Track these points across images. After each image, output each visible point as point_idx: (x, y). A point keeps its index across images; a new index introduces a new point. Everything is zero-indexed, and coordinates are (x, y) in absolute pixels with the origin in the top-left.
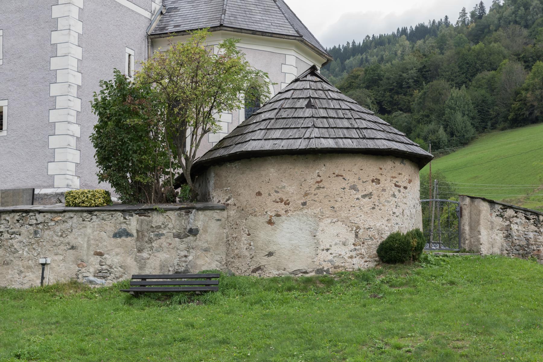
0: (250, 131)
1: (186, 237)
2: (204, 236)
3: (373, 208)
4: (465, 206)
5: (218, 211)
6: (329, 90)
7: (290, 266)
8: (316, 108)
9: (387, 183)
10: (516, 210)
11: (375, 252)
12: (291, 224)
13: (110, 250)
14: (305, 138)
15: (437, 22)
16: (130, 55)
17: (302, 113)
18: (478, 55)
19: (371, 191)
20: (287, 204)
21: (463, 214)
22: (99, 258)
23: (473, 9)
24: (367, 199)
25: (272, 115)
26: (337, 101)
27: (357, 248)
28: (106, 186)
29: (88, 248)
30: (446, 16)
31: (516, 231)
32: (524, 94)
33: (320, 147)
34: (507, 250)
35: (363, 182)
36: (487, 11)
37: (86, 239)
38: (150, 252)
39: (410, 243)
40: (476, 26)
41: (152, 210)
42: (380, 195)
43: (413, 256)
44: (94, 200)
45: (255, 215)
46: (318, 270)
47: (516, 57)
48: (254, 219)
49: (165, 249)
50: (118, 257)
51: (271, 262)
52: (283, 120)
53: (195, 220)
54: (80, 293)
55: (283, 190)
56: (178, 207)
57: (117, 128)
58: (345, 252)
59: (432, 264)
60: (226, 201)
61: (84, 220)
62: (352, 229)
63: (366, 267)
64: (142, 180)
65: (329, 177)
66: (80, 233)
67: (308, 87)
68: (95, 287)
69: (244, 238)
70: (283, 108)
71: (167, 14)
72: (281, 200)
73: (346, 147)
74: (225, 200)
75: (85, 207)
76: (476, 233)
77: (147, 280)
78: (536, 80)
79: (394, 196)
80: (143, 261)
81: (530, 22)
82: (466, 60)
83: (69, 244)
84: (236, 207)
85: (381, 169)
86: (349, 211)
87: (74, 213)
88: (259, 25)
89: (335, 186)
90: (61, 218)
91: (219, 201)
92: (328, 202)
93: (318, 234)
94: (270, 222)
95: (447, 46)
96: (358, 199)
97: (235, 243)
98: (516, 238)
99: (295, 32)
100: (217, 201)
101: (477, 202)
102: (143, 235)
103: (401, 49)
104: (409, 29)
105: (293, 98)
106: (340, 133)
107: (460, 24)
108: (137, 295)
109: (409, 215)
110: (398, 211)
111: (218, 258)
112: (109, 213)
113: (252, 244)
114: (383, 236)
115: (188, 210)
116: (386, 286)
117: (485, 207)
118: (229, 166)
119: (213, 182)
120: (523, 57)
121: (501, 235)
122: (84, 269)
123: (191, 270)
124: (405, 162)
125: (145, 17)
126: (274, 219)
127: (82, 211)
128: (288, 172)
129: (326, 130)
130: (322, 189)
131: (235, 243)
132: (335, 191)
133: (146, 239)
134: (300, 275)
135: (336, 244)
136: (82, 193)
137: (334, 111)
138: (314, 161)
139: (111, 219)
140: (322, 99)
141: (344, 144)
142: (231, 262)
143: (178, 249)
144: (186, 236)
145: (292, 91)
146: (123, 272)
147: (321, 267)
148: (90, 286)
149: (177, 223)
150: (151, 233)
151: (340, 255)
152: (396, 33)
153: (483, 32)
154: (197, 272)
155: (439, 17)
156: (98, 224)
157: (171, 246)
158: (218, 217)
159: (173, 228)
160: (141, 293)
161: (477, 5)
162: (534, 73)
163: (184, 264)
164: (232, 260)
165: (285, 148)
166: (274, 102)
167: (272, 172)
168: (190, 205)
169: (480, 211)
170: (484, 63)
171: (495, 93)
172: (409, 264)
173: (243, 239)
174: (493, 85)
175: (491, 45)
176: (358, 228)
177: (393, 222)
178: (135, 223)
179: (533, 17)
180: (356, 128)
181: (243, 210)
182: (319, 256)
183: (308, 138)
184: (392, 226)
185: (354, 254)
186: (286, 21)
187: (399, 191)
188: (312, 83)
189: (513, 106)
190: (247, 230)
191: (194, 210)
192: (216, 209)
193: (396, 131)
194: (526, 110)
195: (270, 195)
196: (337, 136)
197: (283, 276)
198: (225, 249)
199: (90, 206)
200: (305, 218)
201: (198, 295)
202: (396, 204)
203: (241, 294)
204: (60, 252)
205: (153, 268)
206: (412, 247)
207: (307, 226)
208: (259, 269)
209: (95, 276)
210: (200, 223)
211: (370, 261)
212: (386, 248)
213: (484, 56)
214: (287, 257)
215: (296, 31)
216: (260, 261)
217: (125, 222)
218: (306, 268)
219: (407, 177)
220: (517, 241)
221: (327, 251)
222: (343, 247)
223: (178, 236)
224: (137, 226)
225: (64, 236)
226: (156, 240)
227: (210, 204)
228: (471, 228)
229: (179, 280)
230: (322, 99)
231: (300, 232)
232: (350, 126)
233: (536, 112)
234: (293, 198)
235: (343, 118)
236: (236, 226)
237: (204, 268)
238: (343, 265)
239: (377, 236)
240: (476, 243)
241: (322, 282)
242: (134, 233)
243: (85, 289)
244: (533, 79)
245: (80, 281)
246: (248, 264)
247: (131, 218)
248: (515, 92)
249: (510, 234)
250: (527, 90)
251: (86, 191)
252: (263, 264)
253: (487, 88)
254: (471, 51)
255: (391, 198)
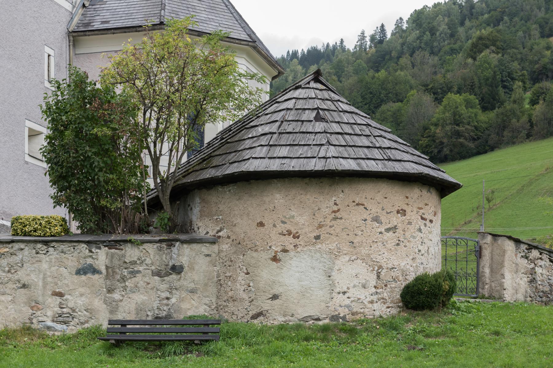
0: (247, 147)
1: (167, 276)
2: (190, 274)
3: (398, 244)
4: (486, 246)
5: (207, 245)
6: (339, 101)
7: (299, 311)
8: (327, 122)
9: (413, 215)
10: (541, 250)
11: (398, 296)
12: (301, 262)
13: (80, 290)
14: (319, 158)
15: (331, 45)
16: (49, 56)
17: (311, 128)
18: (383, 84)
19: (396, 224)
20: (296, 237)
21: (483, 254)
22: (58, 299)
23: (373, 32)
24: (391, 233)
25: (274, 128)
26: (350, 115)
27: (378, 291)
28: (62, 212)
29: (44, 287)
30: (342, 40)
31: (540, 275)
32: (433, 129)
33: (340, 168)
34: (530, 297)
35: (387, 213)
36: (389, 35)
37: (41, 276)
38: (123, 293)
39: (442, 286)
40: (377, 52)
41: (126, 241)
42: (406, 229)
43: (443, 301)
44: (50, 229)
45: (256, 251)
46: (333, 316)
47: (424, 88)
48: (254, 254)
49: (142, 290)
50: (83, 299)
51: (276, 307)
52: (288, 135)
53: (179, 255)
54: (37, 341)
55: (291, 220)
56: (158, 238)
57: (77, 139)
58: (365, 295)
59: (463, 311)
60: (217, 233)
61: (37, 253)
62: (373, 268)
63: (388, 314)
64: (109, 205)
65: (348, 206)
66: (33, 269)
67: (314, 96)
68: (54, 335)
69: (241, 277)
70: (286, 121)
71: (90, 7)
72: (289, 233)
73: (370, 170)
74: (215, 232)
75: (38, 236)
76: (498, 276)
77: (128, 326)
78: (447, 114)
79: (420, 230)
80: (114, 303)
81: (436, 50)
82: (369, 89)
83: (19, 281)
84: (230, 240)
85: (407, 197)
86: (371, 247)
87: (25, 244)
88: (205, 25)
89: (354, 217)
90: (8, 250)
91: (207, 233)
92: (346, 236)
93: (333, 274)
94: (275, 259)
95: (346, 73)
96: (381, 233)
97: (229, 283)
98: (539, 283)
99: (247, 36)
100: (205, 232)
101: (500, 240)
102: (114, 272)
103: (292, 74)
104: (300, 52)
105: (296, 109)
106: (362, 153)
107: (358, 49)
108: (118, 344)
109: (433, 253)
110: (423, 249)
111: (206, 301)
112: (70, 245)
113: (251, 284)
114: (407, 277)
115: (170, 243)
116: (420, 337)
117: (510, 246)
118: (220, 189)
119: (198, 209)
120: (432, 88)
121: (526, 279)
122: (39, 312)
123: (175, 315)
124: (431, 190)
125: (66, 10)
126: (280, 255)
127: (36, 242)
128: (299, 198)
129: (343, 148)
130: (339, 221)
131: (229, 283)
132: (354, 223)
133: (118, 277)
134: (311, 322)
135: (354, 286)
136: (34, 220)
137: (349, 126)
138: (330, 186)
139: (73, 252)
140: (332, 110)
141: (367, 166)
142: (224, 306)
143: (158, 290)
144: (168, 274)
145: (294, 100)
146: (90, 316)
147: (337, 313)
148: (48, 332)
149: (156, 258)
150: (124, 270)
151: (359, 299)
152: (285, 56)
153: (384, 59)
154: (181, 317)
155: (332, 40)
156: (57, 258)
157: (149, 286)
158: (207, 252)
159: (152, 264)
160: (122, 341)
161: (377, 28)
162: (445, 107)
163: (165, 308)
164: (225, 304)
165: (297, 169)
166: (272, 113)
167: (277, 198)
168: (172, 236)
169: (504, 252)
170: (390, 93)
171: (401, 128)
172: (438, 310)
173: (240, 278)
174: (399, 119)
175: (397, 73)
176: (380, 267)
177: (418, 261)
178: (104, 257)
179: (439, 44)
180: (378, 148)
181: (239, 243)
182: (334, 300)
183: (324, 158)
184: (417, 266)
185: (375, 298)
186: (236, 22)
187: (425, 225)
188: (317, 92)
189: (420, 142)
190: (244, 268)
191: (178, 243)
192: (205, 242)
193: (418, 153)
194: (435, 147)
195: (274, 226)
196: (359, 157)
197: (290, 323)
198: (215, 290)
199: (44, 236)
200: (318, 254)
201: (196, 345)
202: (421, 240)
203: (246, 344)
204: (8, 291)
205: (126, 312)
206: (444, 291)
207: (321, 265)
208: (260, 314)
209: (53, 321)
210: (185, 258)
211: (392, 307)
212: (412, 292)
213: (390, 86)
214: (295, 301)
215: (248, 35)
216: (262, 305)
217: (91, 256)
218: (318, 314)
219: (433, 209)
220: (541, 287)
221: (344, 295)
222: (363, 290)
223: (158, 274)
224: (107, 261)
225: (13, 271)
226: (130, 278)
227: (194, 235)
228: (492, 271)
229: (160, 326)
230: (332, 110)
231: (312, 271)
232: (371, 145)
233: (445, 149)
234: (304, 231)
235: (360, 135)
236: (230, 263)
237: (190, 313)
238: (362, 311)
239: (401, 278)
240: (498, 288)
241: (342, 331)
242: (103, 269)
243: (42, 336)
244: (444, 113)
245: (33, 326)
246: (246, 309)
247: (99, 251)
248: (424, 127)
249: (534, 279)
250: (436, 125)
251: (39, 217)
252: (266, 308)
253: (392, 122)
254: (375, 79)
255: (417, 233)
